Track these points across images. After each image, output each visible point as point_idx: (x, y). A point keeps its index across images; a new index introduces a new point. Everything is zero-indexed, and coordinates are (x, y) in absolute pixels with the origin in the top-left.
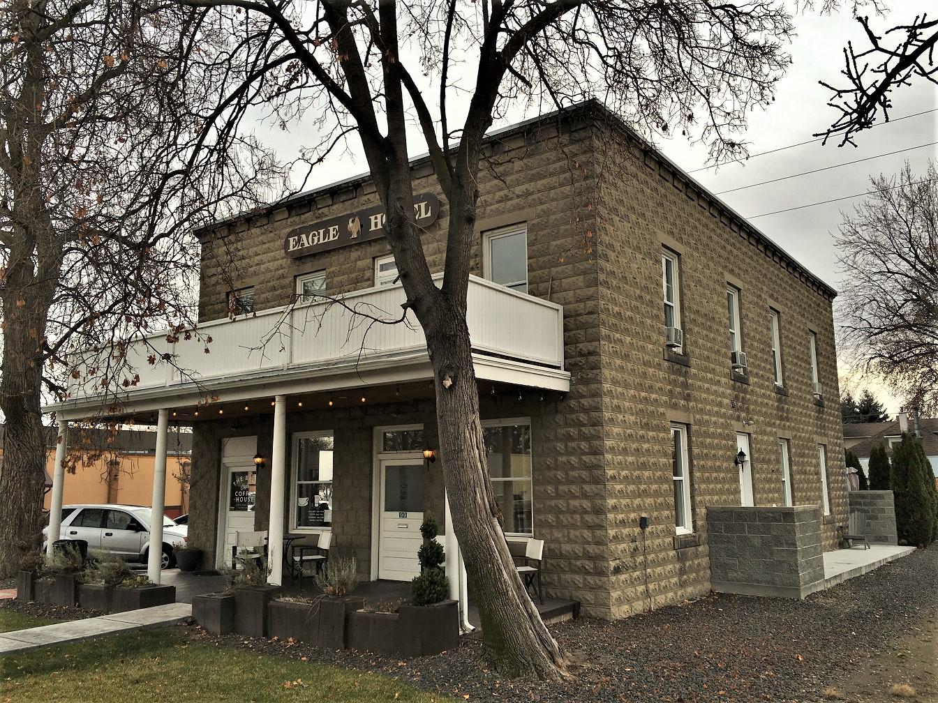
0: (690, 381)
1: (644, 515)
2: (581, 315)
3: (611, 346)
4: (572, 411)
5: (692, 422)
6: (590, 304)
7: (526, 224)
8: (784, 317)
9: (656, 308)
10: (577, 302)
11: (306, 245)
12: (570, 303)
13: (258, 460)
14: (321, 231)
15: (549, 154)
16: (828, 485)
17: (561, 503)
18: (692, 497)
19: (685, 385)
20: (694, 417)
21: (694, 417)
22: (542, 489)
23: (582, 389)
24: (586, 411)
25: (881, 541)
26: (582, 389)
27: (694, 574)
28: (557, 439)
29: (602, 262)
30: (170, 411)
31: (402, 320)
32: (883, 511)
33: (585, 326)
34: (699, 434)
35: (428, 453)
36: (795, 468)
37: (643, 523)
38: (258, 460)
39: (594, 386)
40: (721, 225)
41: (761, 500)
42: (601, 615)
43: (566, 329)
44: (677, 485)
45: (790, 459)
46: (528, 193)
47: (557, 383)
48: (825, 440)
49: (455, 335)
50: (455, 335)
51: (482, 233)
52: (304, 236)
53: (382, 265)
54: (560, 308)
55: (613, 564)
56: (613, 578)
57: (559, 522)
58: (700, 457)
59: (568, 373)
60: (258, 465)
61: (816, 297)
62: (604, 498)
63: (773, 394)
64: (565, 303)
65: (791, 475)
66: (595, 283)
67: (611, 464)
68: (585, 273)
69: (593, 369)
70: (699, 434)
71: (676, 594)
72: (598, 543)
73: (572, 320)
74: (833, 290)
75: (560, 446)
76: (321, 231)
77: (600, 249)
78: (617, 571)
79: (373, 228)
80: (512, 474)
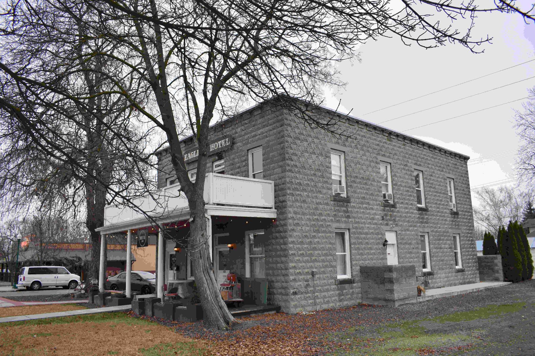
0: (349, 209)
1: (314, 270)
2: (280, 185)
3: (293, 198)
4: (277, 226)
5: (351, 227)
6: (283, 180)
7: (261, 147)
8: (426, 173)
9: (326, 178)
10: (279, 179)
11: (190, 158)
12: (277, 180)
13: (176, 249)
14: (195, 152)
15: (270, 116)
16: (461, 253)
17: (274, 265)
18: (351, 262)
19: (347, 212)
20: (353, 226)
21: (353, 226)
22: (268, 260)
23: (281, 217)
24: (282, 226)
25: (104, 279)
26: (281, 217)
27: (350, 296)
28: (273, 238)
29: (289, 162)
30: (132, 230)
31: (180, 196)
32: (496, 265)
33: (282, 189)
34: (354, 233)
35: (229, 245)
36: (432, 246)
37: (313, 274)
38: (176, 249)
39: (285, 215)
40: (376, 134)
41: (403, 262)
42: (287, 312)
43: (275, 191)
44: (424, 254)
45: (429, 242)
46: (262, 133)
47: (271, 214)
48: (459, 231)
49: (196, 201)
50: (196, 201)
51: (248, 150)
52: (189, 154)
53: (216, 166)
54: (273, 182)
55: (292, 291)
56: (293, 297)
57: (273, 273)
58: (355, 244)
59: (276, 210)
60: (176, 251)
61: (459, 162)
62: (288, 263)
63: (416, 211)
64: (275, 180)
65: (430, 250)
66: (284, 171)
67: (291, 249)
68: (281, 167)
69: (284, 208)
70: (354, 233)
71: (336, 304)
72: (286, 282)
73: (277, 187)
74: (466, 156)
75: (273, 241)
76: (195, 152)
77: (287, 156)
78: (295, 293)
79: (211, 150)
80: (123, 259)
